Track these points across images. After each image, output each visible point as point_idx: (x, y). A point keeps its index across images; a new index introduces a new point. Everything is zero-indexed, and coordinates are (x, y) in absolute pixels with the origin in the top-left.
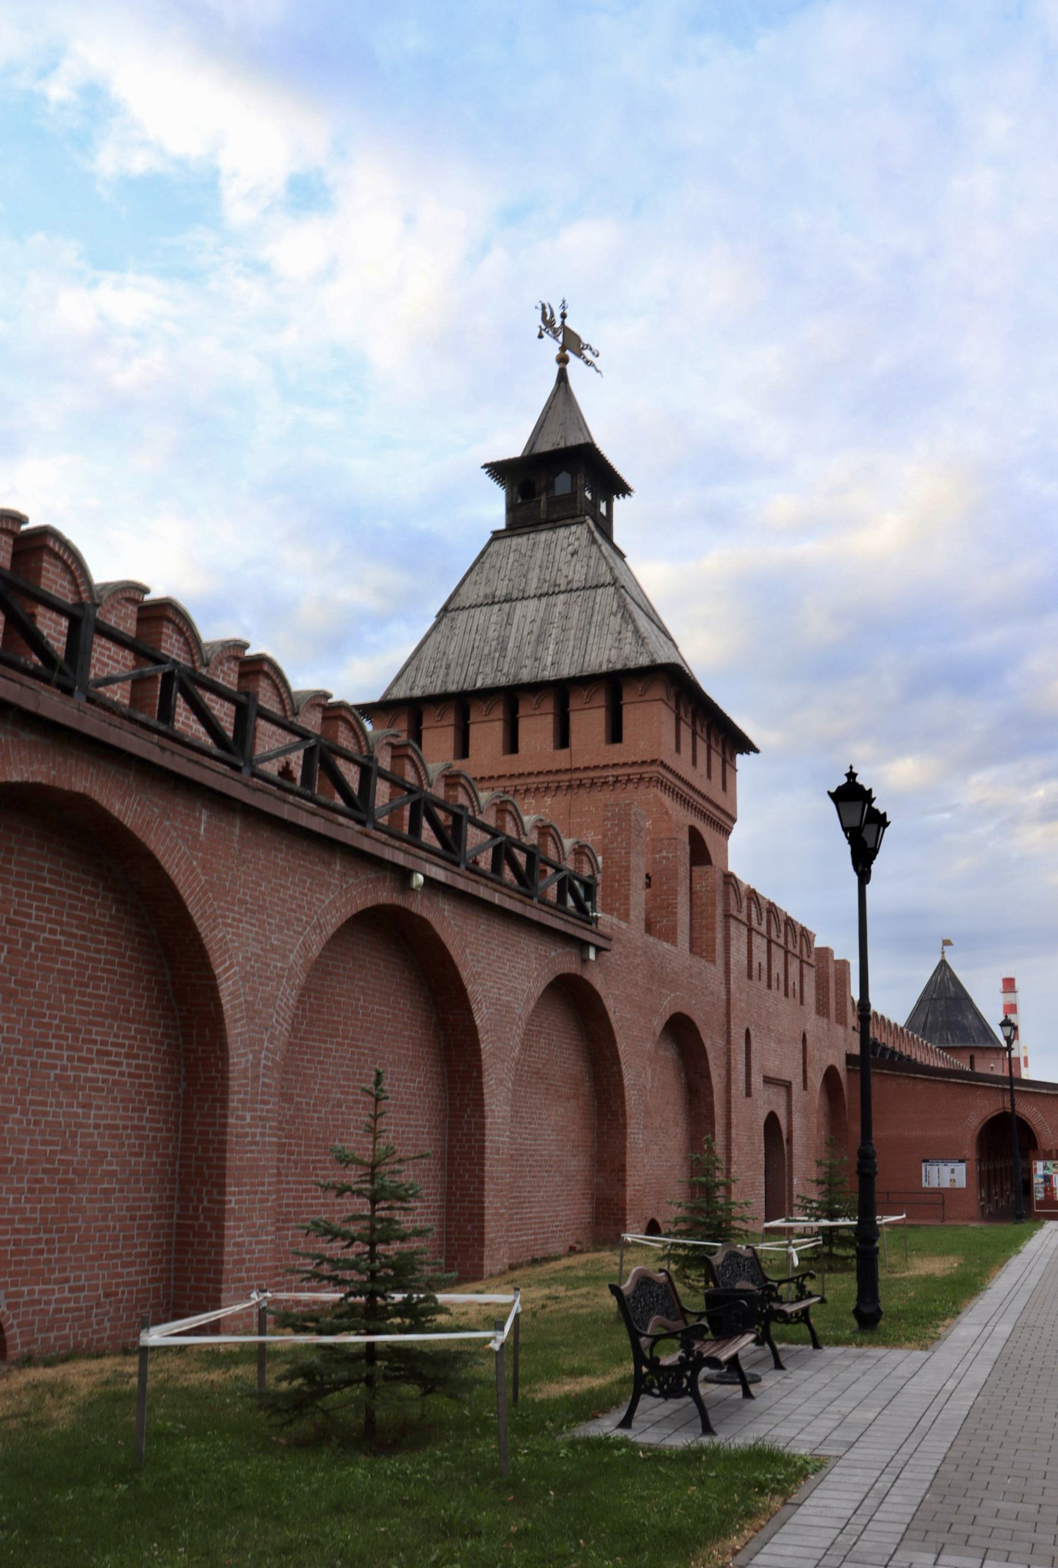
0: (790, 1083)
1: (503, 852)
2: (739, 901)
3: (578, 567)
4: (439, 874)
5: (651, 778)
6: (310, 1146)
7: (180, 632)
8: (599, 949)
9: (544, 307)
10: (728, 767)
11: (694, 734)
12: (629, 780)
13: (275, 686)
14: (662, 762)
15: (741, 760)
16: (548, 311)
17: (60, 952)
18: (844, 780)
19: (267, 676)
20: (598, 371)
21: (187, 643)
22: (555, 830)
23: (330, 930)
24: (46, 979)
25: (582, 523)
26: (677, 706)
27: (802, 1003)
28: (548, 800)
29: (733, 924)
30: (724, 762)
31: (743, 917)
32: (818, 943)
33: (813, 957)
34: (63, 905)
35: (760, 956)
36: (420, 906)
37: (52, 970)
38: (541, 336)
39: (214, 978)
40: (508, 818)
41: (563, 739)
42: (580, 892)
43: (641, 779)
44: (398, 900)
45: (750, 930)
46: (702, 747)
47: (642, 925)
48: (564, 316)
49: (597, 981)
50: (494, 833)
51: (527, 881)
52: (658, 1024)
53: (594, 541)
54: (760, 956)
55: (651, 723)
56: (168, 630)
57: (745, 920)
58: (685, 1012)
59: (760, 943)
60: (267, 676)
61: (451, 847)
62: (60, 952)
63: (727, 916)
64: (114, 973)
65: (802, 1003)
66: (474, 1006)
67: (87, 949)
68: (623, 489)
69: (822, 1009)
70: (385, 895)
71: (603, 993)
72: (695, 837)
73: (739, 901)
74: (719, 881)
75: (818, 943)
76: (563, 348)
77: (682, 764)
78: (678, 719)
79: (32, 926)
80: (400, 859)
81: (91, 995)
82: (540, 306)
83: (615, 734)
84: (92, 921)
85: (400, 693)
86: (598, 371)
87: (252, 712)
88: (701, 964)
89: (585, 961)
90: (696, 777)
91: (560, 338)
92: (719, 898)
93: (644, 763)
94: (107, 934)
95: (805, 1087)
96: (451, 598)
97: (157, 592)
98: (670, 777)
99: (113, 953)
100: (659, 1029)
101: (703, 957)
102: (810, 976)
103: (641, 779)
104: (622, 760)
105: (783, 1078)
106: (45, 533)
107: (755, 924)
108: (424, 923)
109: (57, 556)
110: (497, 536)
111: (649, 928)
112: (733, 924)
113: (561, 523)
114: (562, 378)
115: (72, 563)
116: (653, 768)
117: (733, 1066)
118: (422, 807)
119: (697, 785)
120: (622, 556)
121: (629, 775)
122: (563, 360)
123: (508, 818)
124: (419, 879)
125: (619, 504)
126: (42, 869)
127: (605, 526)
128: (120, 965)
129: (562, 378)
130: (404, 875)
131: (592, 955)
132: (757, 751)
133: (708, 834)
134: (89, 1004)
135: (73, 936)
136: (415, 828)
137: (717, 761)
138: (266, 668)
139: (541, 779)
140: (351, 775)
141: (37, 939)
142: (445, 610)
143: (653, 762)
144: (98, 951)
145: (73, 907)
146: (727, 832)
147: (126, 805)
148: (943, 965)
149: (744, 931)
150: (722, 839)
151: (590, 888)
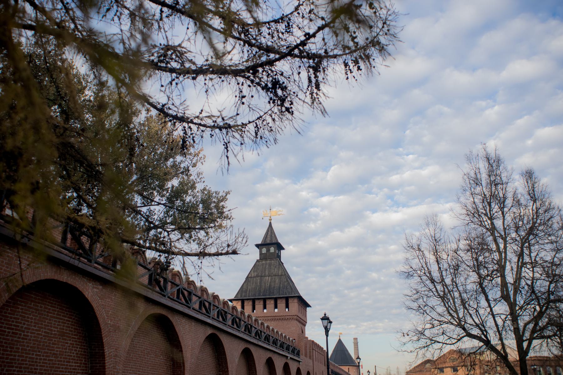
15: (308, 309)
55: (294, 305)
125: (282, 251)
127: (279, 257)
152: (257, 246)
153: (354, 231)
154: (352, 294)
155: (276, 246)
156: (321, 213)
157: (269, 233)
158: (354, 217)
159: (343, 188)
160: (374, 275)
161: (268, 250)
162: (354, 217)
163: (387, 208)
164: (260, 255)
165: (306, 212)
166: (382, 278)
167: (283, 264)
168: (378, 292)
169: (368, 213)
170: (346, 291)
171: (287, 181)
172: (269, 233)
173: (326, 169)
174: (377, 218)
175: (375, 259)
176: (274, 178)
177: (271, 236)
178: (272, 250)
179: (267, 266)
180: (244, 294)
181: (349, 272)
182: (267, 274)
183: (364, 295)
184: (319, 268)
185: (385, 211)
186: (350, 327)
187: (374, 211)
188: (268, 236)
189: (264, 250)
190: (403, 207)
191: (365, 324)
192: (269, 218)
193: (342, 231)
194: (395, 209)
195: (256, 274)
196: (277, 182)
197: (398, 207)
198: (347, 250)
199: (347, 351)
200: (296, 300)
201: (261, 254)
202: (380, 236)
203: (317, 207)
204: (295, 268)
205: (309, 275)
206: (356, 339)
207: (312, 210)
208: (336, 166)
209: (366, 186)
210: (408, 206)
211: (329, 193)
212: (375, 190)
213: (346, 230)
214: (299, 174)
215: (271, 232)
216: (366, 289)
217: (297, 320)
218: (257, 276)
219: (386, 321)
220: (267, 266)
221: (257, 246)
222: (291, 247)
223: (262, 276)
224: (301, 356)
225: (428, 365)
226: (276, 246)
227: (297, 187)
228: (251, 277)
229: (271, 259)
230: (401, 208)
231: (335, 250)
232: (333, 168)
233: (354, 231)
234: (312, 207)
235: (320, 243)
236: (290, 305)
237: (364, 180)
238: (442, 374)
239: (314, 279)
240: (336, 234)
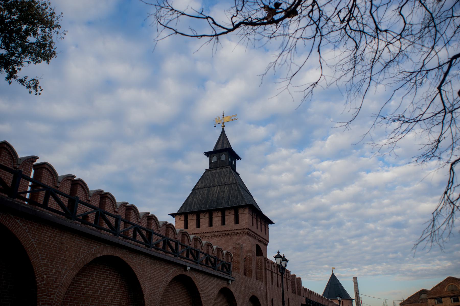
1: (208, 259)
2: (269, 265)
4: (194, 266)
7: (135, 212)
8: (232, 281)
10: (266, 228)
11: (257, 221)
13: (155, 222)
15: (270, 226)
17: (110, 291)
18: (277, 254)
19: (154, 219)
21: (136, 214)
23: (169, 282)
24: (107, 297)
26: (252, 214)
27: (287, 290)
28: (220, 238)
29: (267, 271)
30: (265, 227)
31: (270, 269)
32: (292, 274)
33: (290, 277)
34: (111, 280)
35: (275, 279)
36: (188, 274)
37: (109, 295)
39: (143, 295)
40: (210, 247)
41: (223, 223)
42: (227, 268)
43: (243, 233)
44: (184, 273)
45: (272, 272)
46: (259, 223)
47: (243, 273)
49: (232, 289)
50: (206, 255)
51: (214, 265)
52: (248, 299)
53: (231, 172)
54: (275, 279)
55: (245, 218)
56: (132, 211)
58: (255, 295)
59: (275, 275)
60: (154, 219)
61: (196, 258)
62: (110, 291)
63: (266, 269)
64: (121, 295)
65: (287, 290)
66: (201, 297)
67: (116, 290)
68: (239, 158)
69: (293, 292)
70: (181, 272)
71: (233, 292)
72: (258, 247)
73: (269, 265)
74: (263, 260)
75: (292, 274)
77: (254, 229)
78: (253, 217)
79: (105, 286)
80: (184, 263)
81: (117, 301)
83: (237, 222)
84: (117, 283)
85: (183, 211)
87: (152, 233)
88: (259, 282)
89: (229, 284)
90: (258, 231)
92: (263, 265)
94: (120, 286)
97: (130, 204)
98: (251, 232)
99: (121, 290)
100: (248, 300)
102: (290, 283)
103: (243, 233)
104: (239, 228)
106: (108, 193)
107: (273, 270)
108: (190, 278)
109: (109, 198)
111: (245, 274)
112: (267, 271)
115: (112, 199)
116: (247, 230)
118: (189, 250)
119: (258, 234)
123: (210, 247)
124: (189, 268)
125: (237, 161)
126: (107, 272)
127: (234, 168)
128: (123, 293)
130: (185, 267)
131: (230, 282)
132: (274, 224)
133: (261, 246)
134: (116, 303)
135: (113, 287)
136: (188, 255)
137: (263, 226)
138: (153, 218)
139: (218, 233)
140: (173, 244)
141: (106, 288)
144: (118, 290)
145: (114, 280)
146: (267, 245)
147: (128, 259)
148: (333, 276)
149: (270, 272)
150: (265, 247)
151: (230, 266)
152: (207, 154)
153: (352, 189)
154: (353, 242)
155: (227, 152)
156: (322, 175)
157: (221, 140)
158: (351, 178)
159: (339, 154)
160: (371, 226)
161: (219, 158)
162: (351, 178)
163: (380, 168)
164: (210, 164)
165: (310, 176)
166: (378, 228)
167: (238, 174)
168: (375, 239)
169: (363, 174)
170: (348, 240)
171: (292, 151)
172: (221, 140)
173: (324, 138)
174: (371, 178)
175: (371, 212)
176: (281, 148)
177: (223, 142)
178: (223, 157)
179: (217, 175)
180: (188, 207)
181: (349, 224)
182: (216, 183)
183: (364, 243)
184: (324, 222)
185: (378, 171)
186: (353, 270)
187: (368, 171)
188: (220, 143)
189: (215, 159)
190: (393, 167)
191: (366, 267)
192: (222, 125)
193: (341, 189)
194: (386, 168)
195: (203, 184)
196: (284, 152)
197: (389, 167)
198: (347, 206)
199: (341, 285)
200: (247, 211)
201: (211, 163)
202: (375, 193)
203: (318, 170)
204: (303, 222)
205: (316, 227)
206: (355, 278)
207: (315, 173)
208: (332, 136)
209: (360, 150)
210: (398, 166)
211: (328, 159)
212: (367, 154)
213: (345, 189)
214: (302, 144)
215: (224, 139)
216: (365, 238)
217: (248, 234)
218: (205, 187)
219: (385, 264)
220: (217, 175)
221: (207, 154)
222: (299, 205)
223: (210, 187)
224: (234, 274)
225: (423, 296)
226: (227, 152)
227: (301, 155)
228: (198, 189)
229: (222, 167)
230: (391, 167)
231: (336, 206)
232: (330, 137)
233: (352, 189)
234: (314, 171)
235: (323, 200)
236: (241, 217)
237: (356, 146)
238: (440, 305)
239: (320, 231)
240: (337, 192)
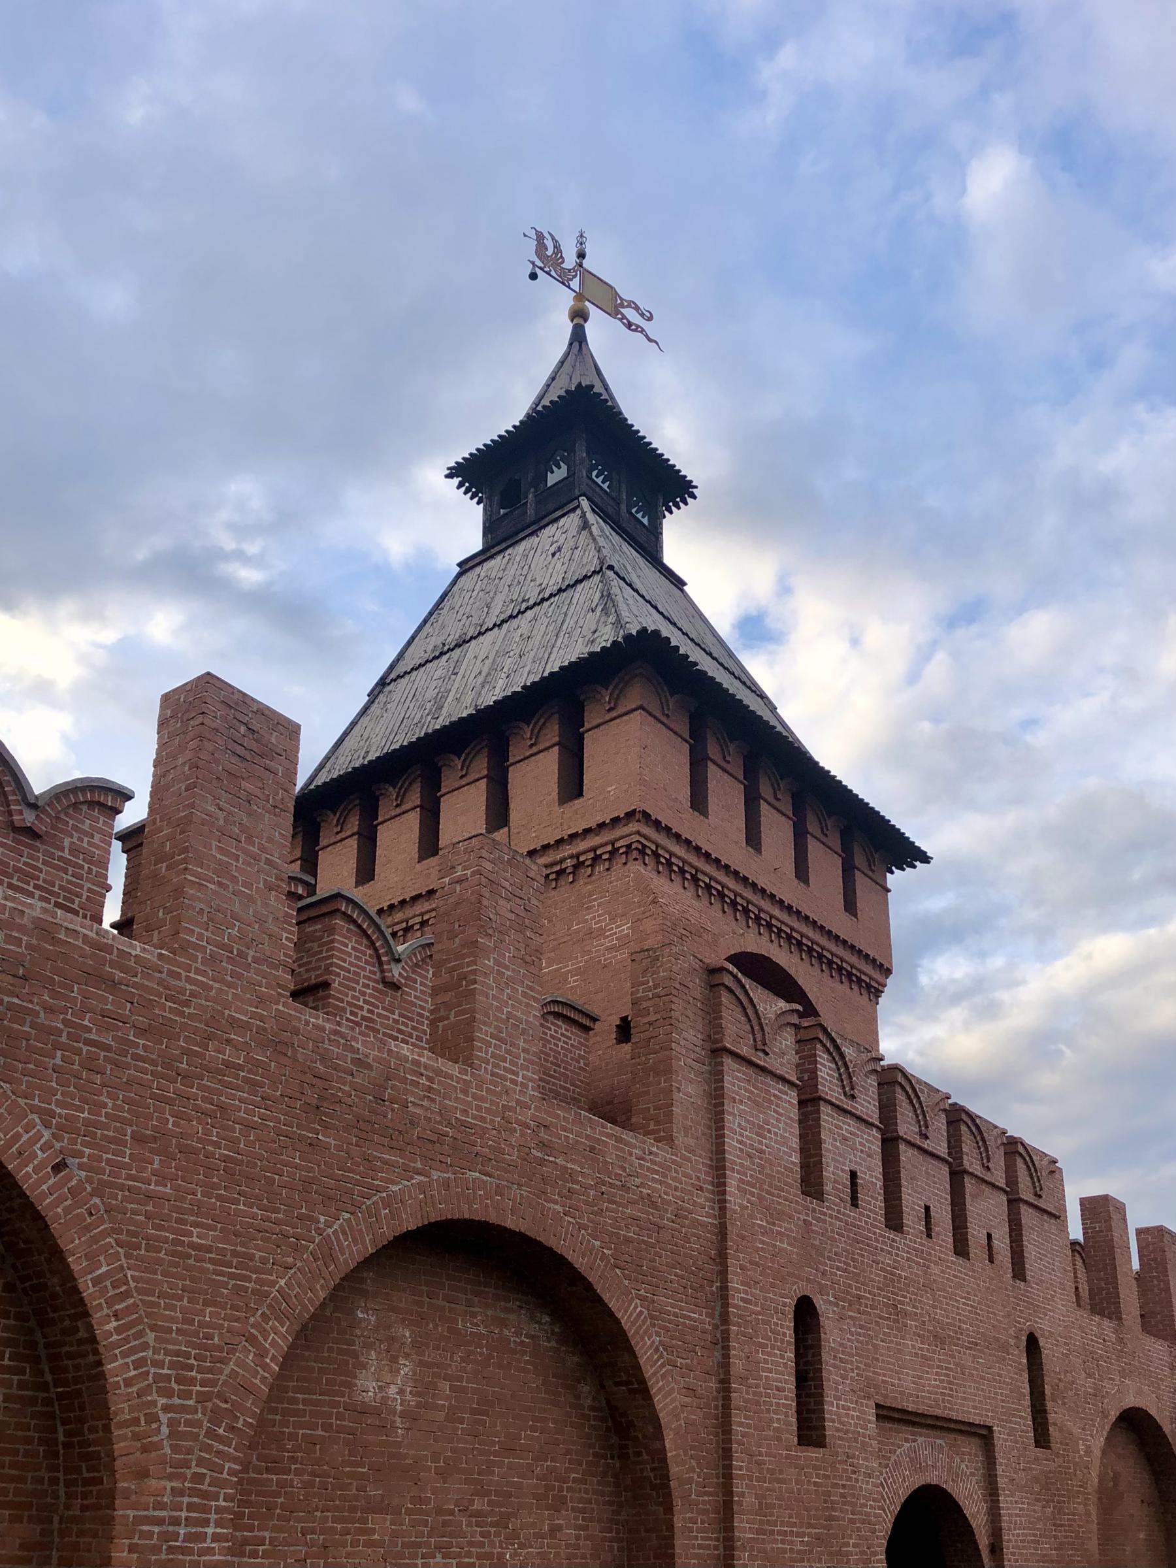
0: (990, 1429)
3: (559, 564)
5: (629, 846)
6: (182, 1493)
9: (540, 237)
12: (596, 859)
14: (646, 815)
15: (896, 879)
16: (549, 244)
20: (650, 340)
22: (350, 901)
25: (574, 510)
38: (533, 276)
48: (581, 255)
57: (1001, 1183)
63: (717, 1051)
76: (580, 297)
82: (533, 234)
86: (650, 340)
91: (575, 284)
93: (616, 821)
95: (1042, 1438)
96: (392, 667)
101: (647, 1133)
105: (954, 1415)
110: (467, 566)
113: (547, 520)
114: (578, 338)
116: (634, 827)
117: (738, 1364)
120: (679, 583)
121: (594, 850)
122: (579, 315)
129: (578, 338)
142: (383, 683)
143: (630, 815)
150: (864, 1000)
